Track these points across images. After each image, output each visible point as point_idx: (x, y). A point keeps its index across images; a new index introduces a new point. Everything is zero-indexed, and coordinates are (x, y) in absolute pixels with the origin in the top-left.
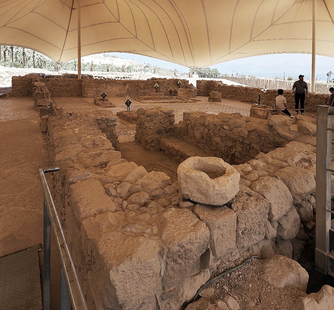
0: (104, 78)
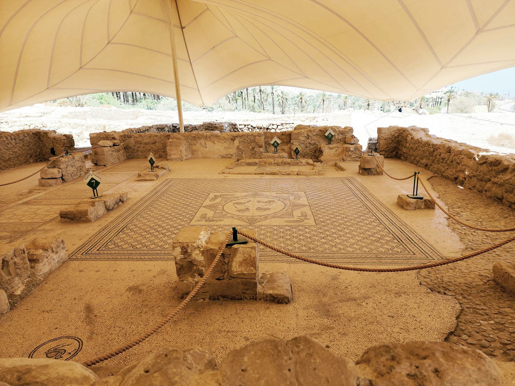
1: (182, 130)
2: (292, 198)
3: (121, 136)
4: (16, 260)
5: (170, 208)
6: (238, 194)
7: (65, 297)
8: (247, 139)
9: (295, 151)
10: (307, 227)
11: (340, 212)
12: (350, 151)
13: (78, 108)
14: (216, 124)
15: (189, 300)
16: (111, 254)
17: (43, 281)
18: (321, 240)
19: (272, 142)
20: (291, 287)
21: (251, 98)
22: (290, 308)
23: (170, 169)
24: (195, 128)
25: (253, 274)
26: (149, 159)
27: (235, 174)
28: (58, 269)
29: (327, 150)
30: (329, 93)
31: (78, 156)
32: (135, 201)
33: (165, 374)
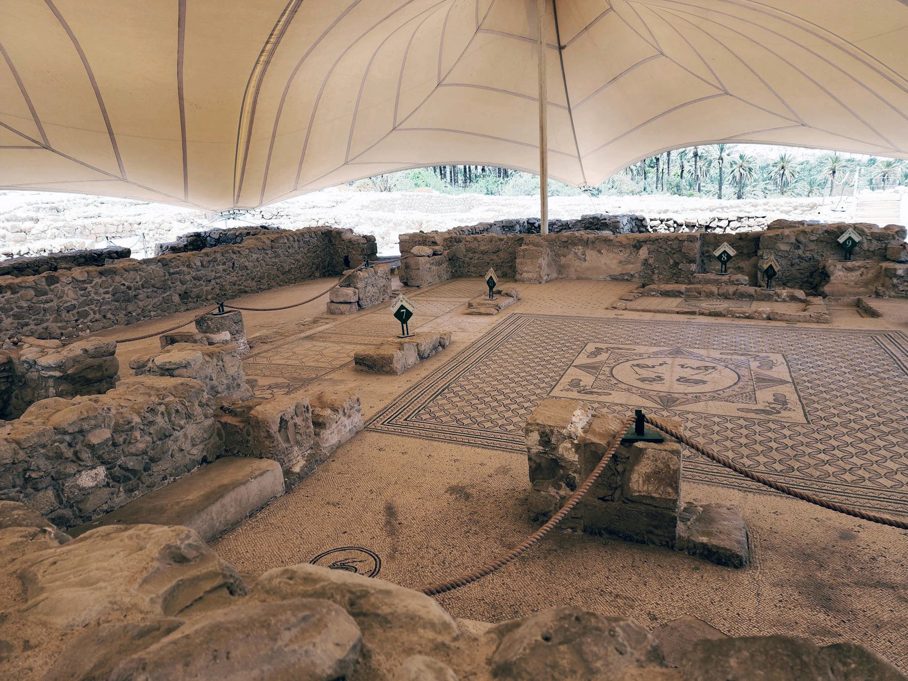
0: (675, 222)
1: (545, 230)
2: (754, 365)
3: (445, 240)
4: (298, 420)
5: (517, 363)
6: (641, 349)
7: (358, 487)
8: (664, 247)
9: (767, 271)
10: (787, 425)
11: (865, 402)
12: (896, 276)
13: (385, 193)
14: (605, 219)
15: (552, 527)
16: (424, 429)
17: (329, 457)
18: (819, 456)
19: (717, 253)
20: (748, 538)
21: (675, 170)
22: (744, 577)
23: (519, 297)
24: (566, 226)
25: (670, 500)
26: (487, 278)
27: (638, 311)
28: (350, 441)
29: (841, 273)
30: (847, 156)
31: (382, 269)
32: (463, 347)
33: (579, 652)
